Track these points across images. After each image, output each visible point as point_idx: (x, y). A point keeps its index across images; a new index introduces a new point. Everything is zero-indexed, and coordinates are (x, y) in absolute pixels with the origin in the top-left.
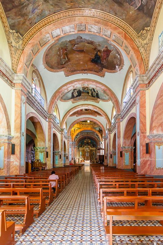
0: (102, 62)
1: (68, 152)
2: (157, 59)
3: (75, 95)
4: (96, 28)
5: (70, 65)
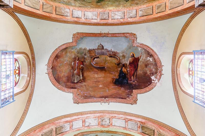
5: (84, 87)
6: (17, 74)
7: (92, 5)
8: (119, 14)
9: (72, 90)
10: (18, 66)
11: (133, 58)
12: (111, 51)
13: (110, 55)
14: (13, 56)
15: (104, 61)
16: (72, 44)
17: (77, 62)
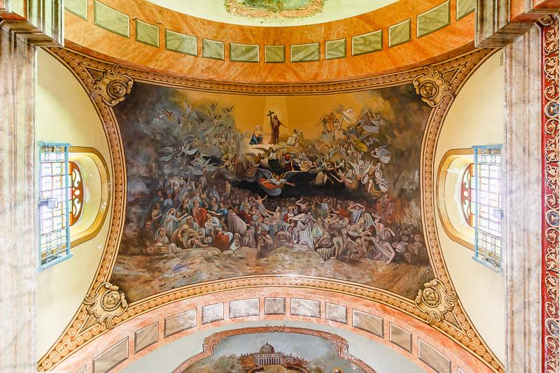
2: (512, 295)
4: (310, 305)
6: (76, 197)
7: (249, 268)
8: (307, 306)
10: (78, 179)
13: (288, 364)
14: (66, 156)
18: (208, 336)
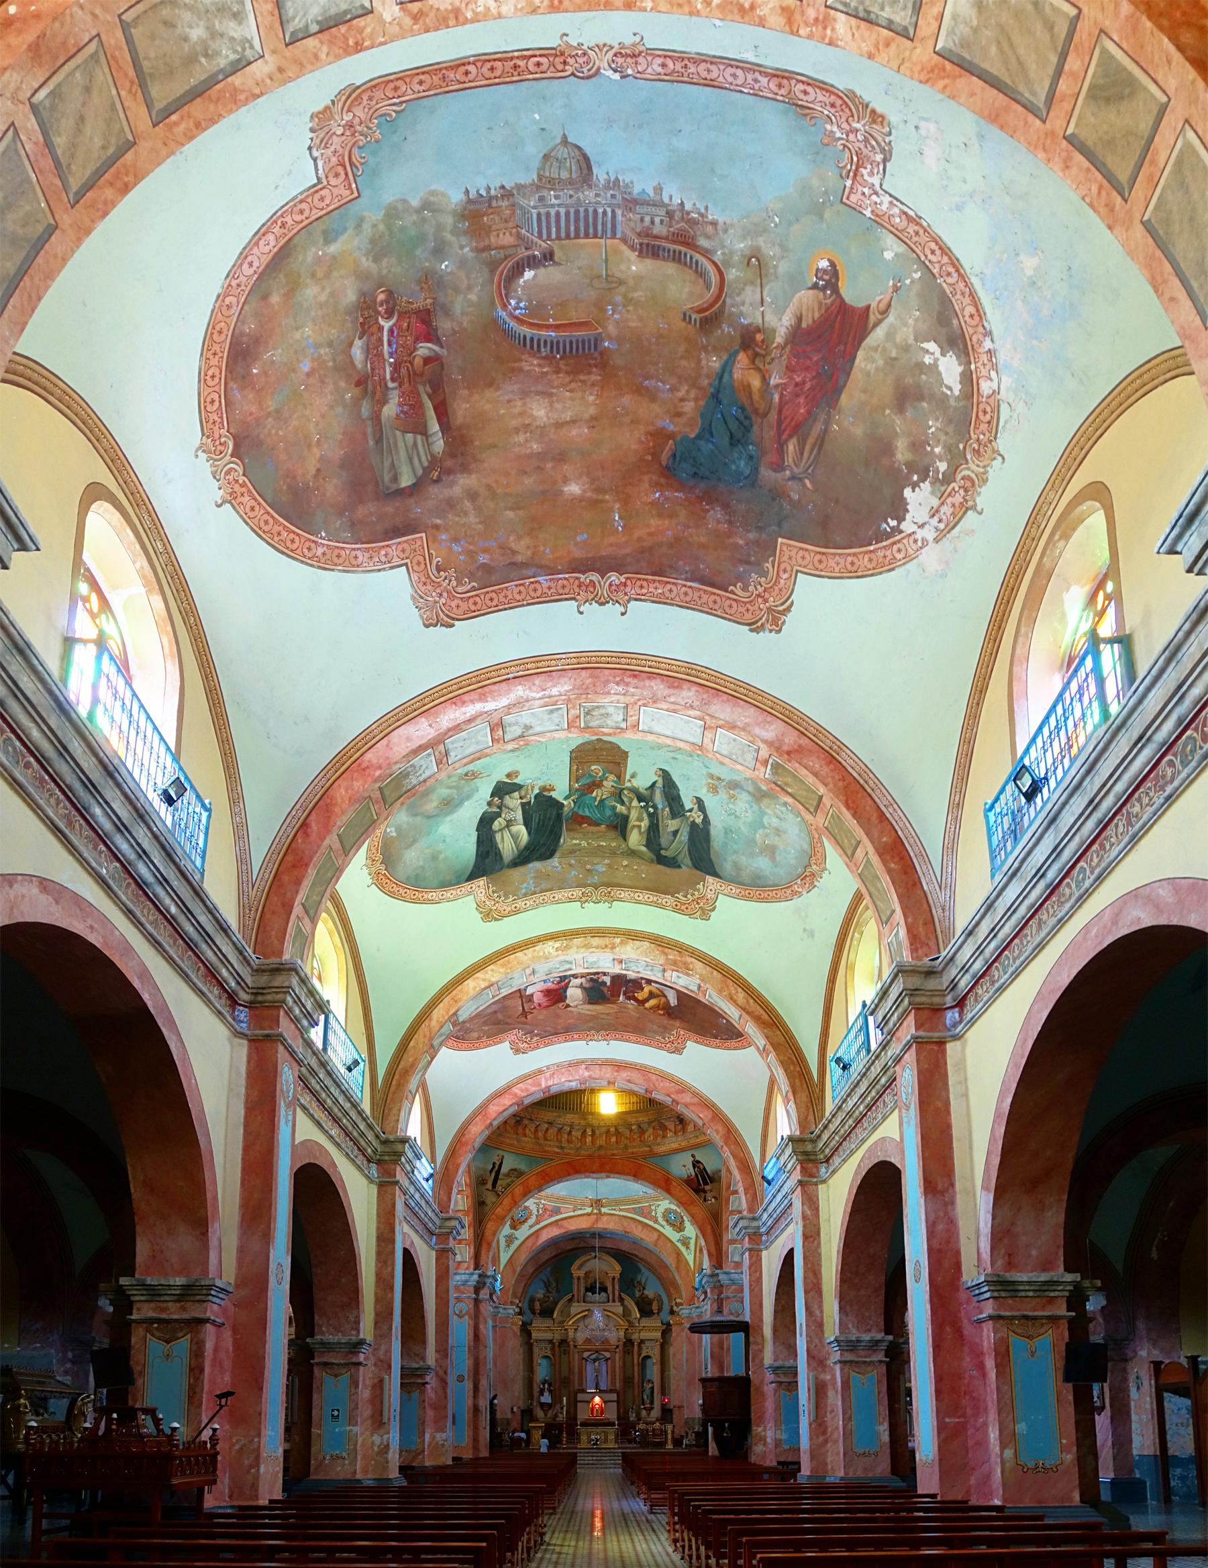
0: (766, 473)
1: (443, 1350)
3: (507, 846)
9: (400, 547)
11: (828, 298)
12: (662, 204)
13: (646, 233)
15: (596, 283)
16: (322, 199)
17: (386, 325)
18: (320, 107)
